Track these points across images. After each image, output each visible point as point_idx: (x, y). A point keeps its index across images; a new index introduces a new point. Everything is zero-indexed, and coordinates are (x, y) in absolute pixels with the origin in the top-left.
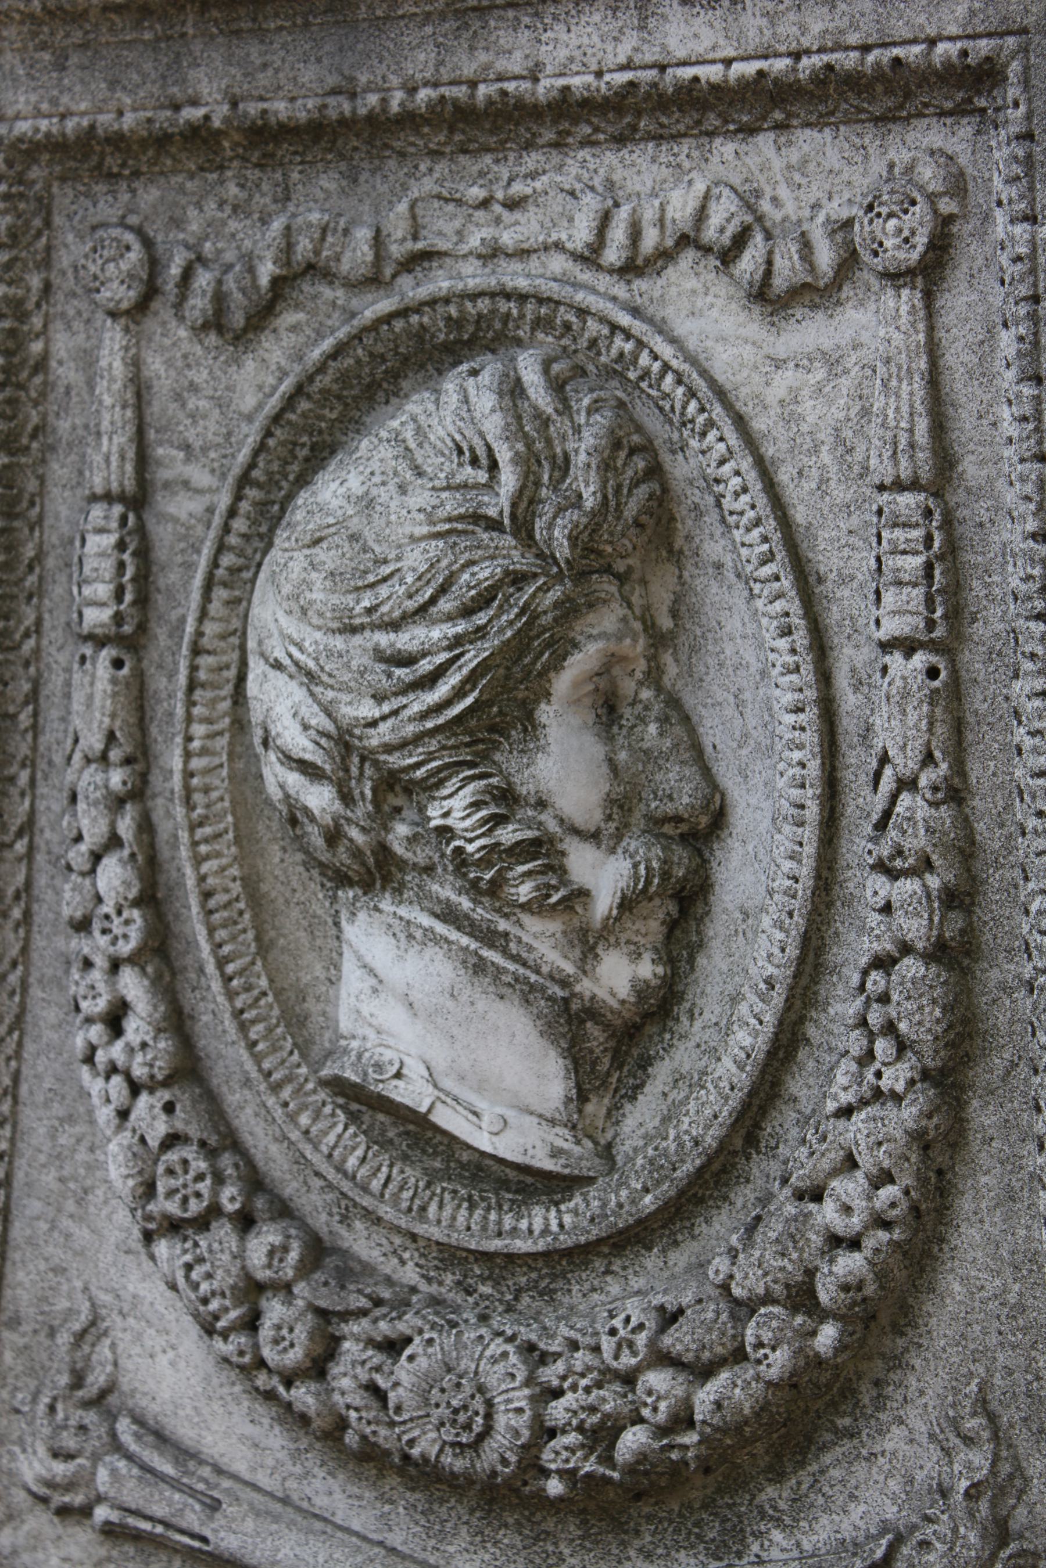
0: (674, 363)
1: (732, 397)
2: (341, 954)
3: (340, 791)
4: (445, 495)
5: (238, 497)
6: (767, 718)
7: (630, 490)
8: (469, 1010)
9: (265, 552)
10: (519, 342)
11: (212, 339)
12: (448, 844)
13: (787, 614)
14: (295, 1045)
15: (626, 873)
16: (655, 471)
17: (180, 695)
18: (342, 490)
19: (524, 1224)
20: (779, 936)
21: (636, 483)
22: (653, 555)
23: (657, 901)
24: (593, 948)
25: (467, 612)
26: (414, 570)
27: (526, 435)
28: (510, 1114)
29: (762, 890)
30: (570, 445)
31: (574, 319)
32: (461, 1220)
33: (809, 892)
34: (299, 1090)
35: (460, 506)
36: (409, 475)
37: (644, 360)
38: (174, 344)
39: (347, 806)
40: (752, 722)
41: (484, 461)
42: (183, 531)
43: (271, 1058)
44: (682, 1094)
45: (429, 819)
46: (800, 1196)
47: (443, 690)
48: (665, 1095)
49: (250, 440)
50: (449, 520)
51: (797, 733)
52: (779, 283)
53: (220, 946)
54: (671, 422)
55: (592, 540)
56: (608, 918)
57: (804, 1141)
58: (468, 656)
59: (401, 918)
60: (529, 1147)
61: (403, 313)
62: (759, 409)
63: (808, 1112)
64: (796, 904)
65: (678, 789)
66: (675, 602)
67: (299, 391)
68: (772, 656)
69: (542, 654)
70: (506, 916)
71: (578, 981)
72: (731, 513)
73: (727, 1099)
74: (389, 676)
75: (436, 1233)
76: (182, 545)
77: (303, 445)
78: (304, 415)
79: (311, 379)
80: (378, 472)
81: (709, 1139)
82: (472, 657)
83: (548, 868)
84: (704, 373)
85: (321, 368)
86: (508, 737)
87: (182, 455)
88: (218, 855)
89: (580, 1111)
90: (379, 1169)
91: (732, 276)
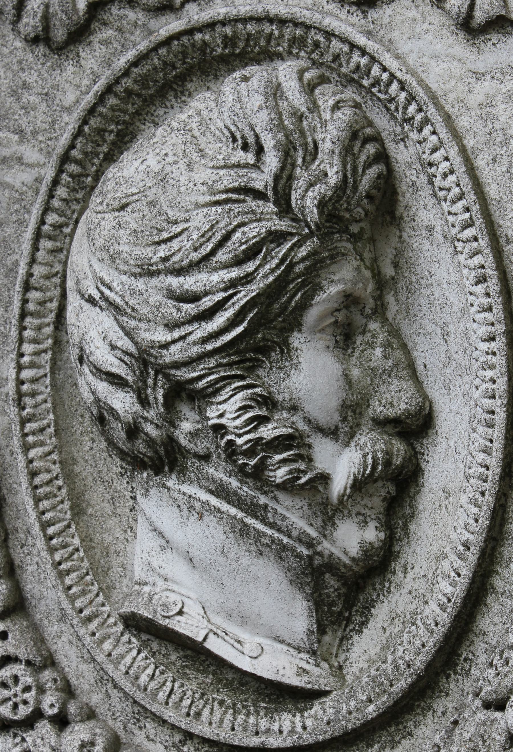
0: (399, 74)
1: (442, 101)
2: (136, 521)
3: (139, 397)
4: (222, 172)
5: (60, 171)
6: (466, 345)
7: (364, 171)
8: (234, 565)
9: (81, 213)
10: (280, 56)
11: (41, 49)
12: (222, 437)
13: (483, 267)
14: (100, 589)
15: (357, 461)
16: (383, 157)
17: (14, 321)
18: (142, 168)
19: (276, 727)
20: (475, 510)
21: (368, 165)
22: (380, 220)
23: (380, 484)
24: (331, 519)
25: (238, 261)
26: (199, 229)
27: (284, 128)
28: (266, 643)
29: (461, 476)
30: (319, 136)
31: (322, 39)
32: (227, 723)
33: (497, 478)
34: (103, 624)
35: (234, 181)
36: (195, 156)
37: (375, 70)
38: (11, 52)
39: (144, 407)
40: (454, 348)
41: (253, 148)
42: (17, 195)
43: (82, 599)
44: (397, 629)
45: (209, 419)
46: (487, 706)
47: (220, 320)
48: (384, 629)
49: (70, 127)
50: (227, 191)
51: (489, 357)
52: (480, 16)
53: (43, 513)
54: (394, 118)
55: (335, 208)
56: (343, 496)
57: (491, 664)
58: (239, 296)
59: (184, 494)
60: (280, 668)
61: (190, 32)
62: (463, 110)
63: (494, 643)
64: (486, 486)
65: (396, 398)
66: (396, 256)
67: (109, 90)
68: (471, 298)
69: (295, 294)
70: (266, 493)
71: (319, 543)
72: (441, 189)
73: (432, 633)
74: (179, 310)
75: (208, 732)
76: (17, 206)
77: (111, 132)
78: (112, 109)
79: (117, 81)
80: (170, 154)
81: (419, 664)
82: (244, 295)
83: (299, 457)
84: (421, 82)
85: (126, 73)
86: (269, 357)
87: (16, 137)
88: (42, 444)
89: (319, 641)
90: (164, 684)
91: (443, 9)
